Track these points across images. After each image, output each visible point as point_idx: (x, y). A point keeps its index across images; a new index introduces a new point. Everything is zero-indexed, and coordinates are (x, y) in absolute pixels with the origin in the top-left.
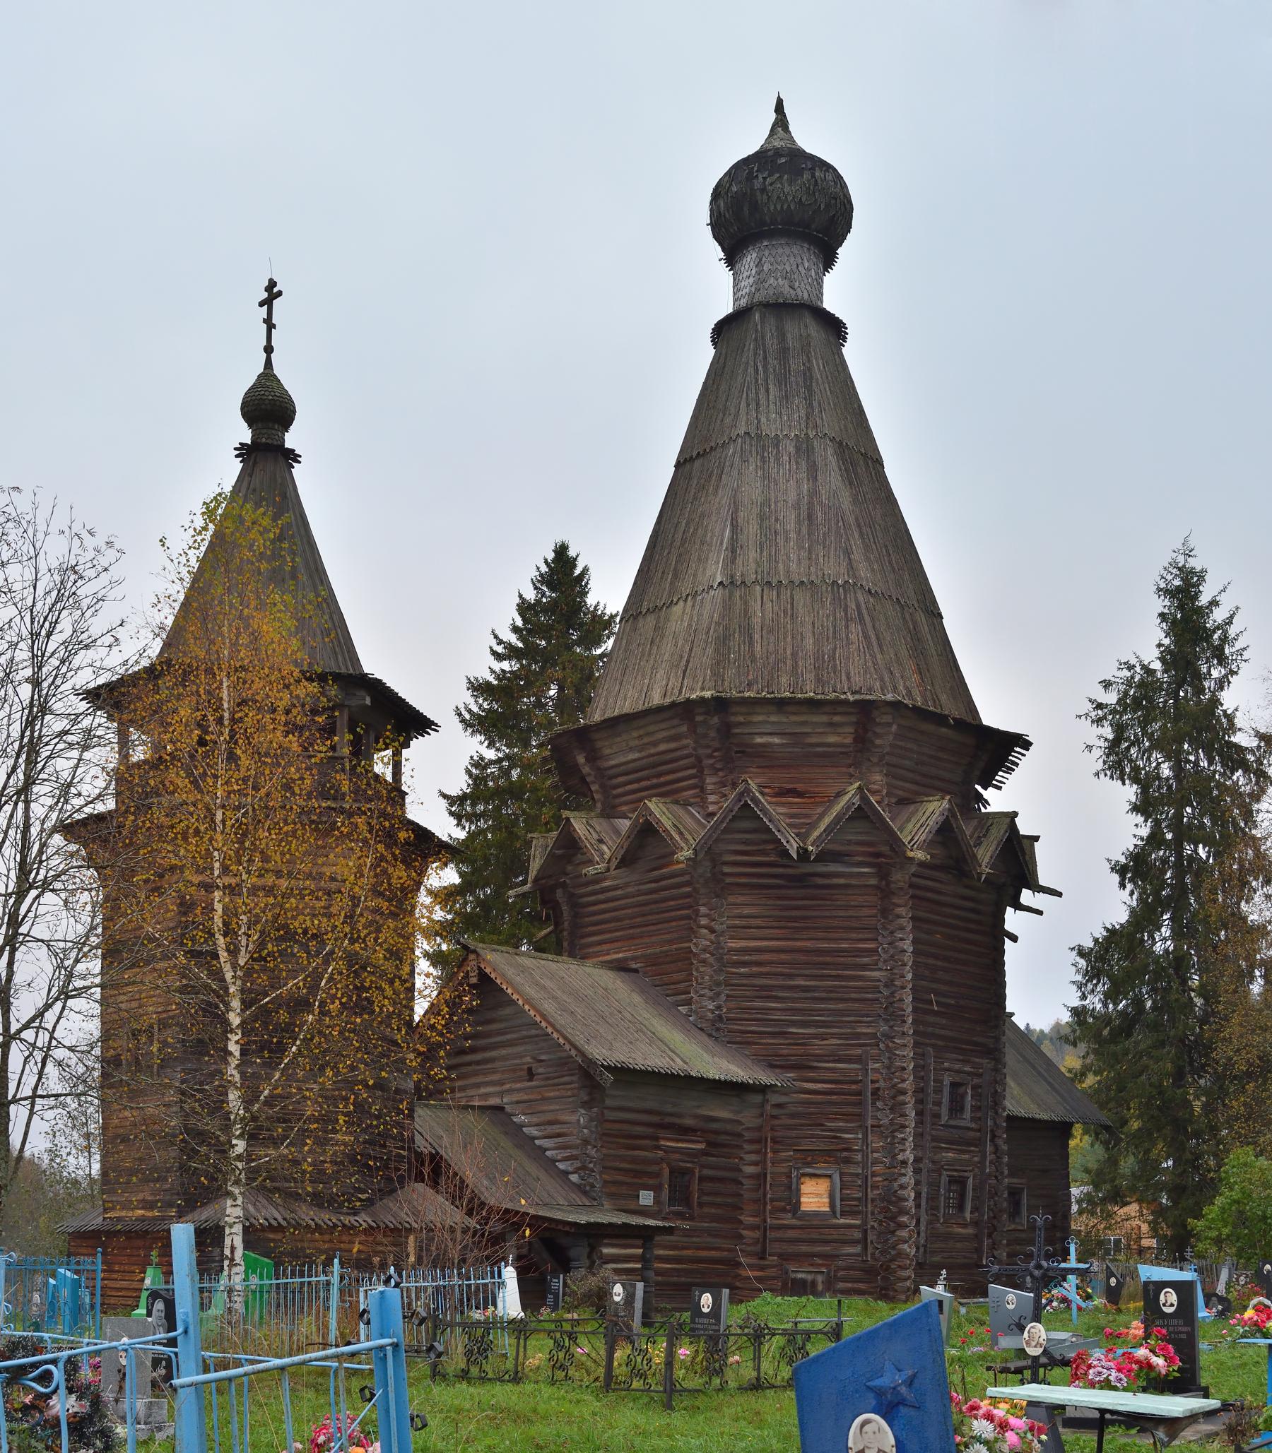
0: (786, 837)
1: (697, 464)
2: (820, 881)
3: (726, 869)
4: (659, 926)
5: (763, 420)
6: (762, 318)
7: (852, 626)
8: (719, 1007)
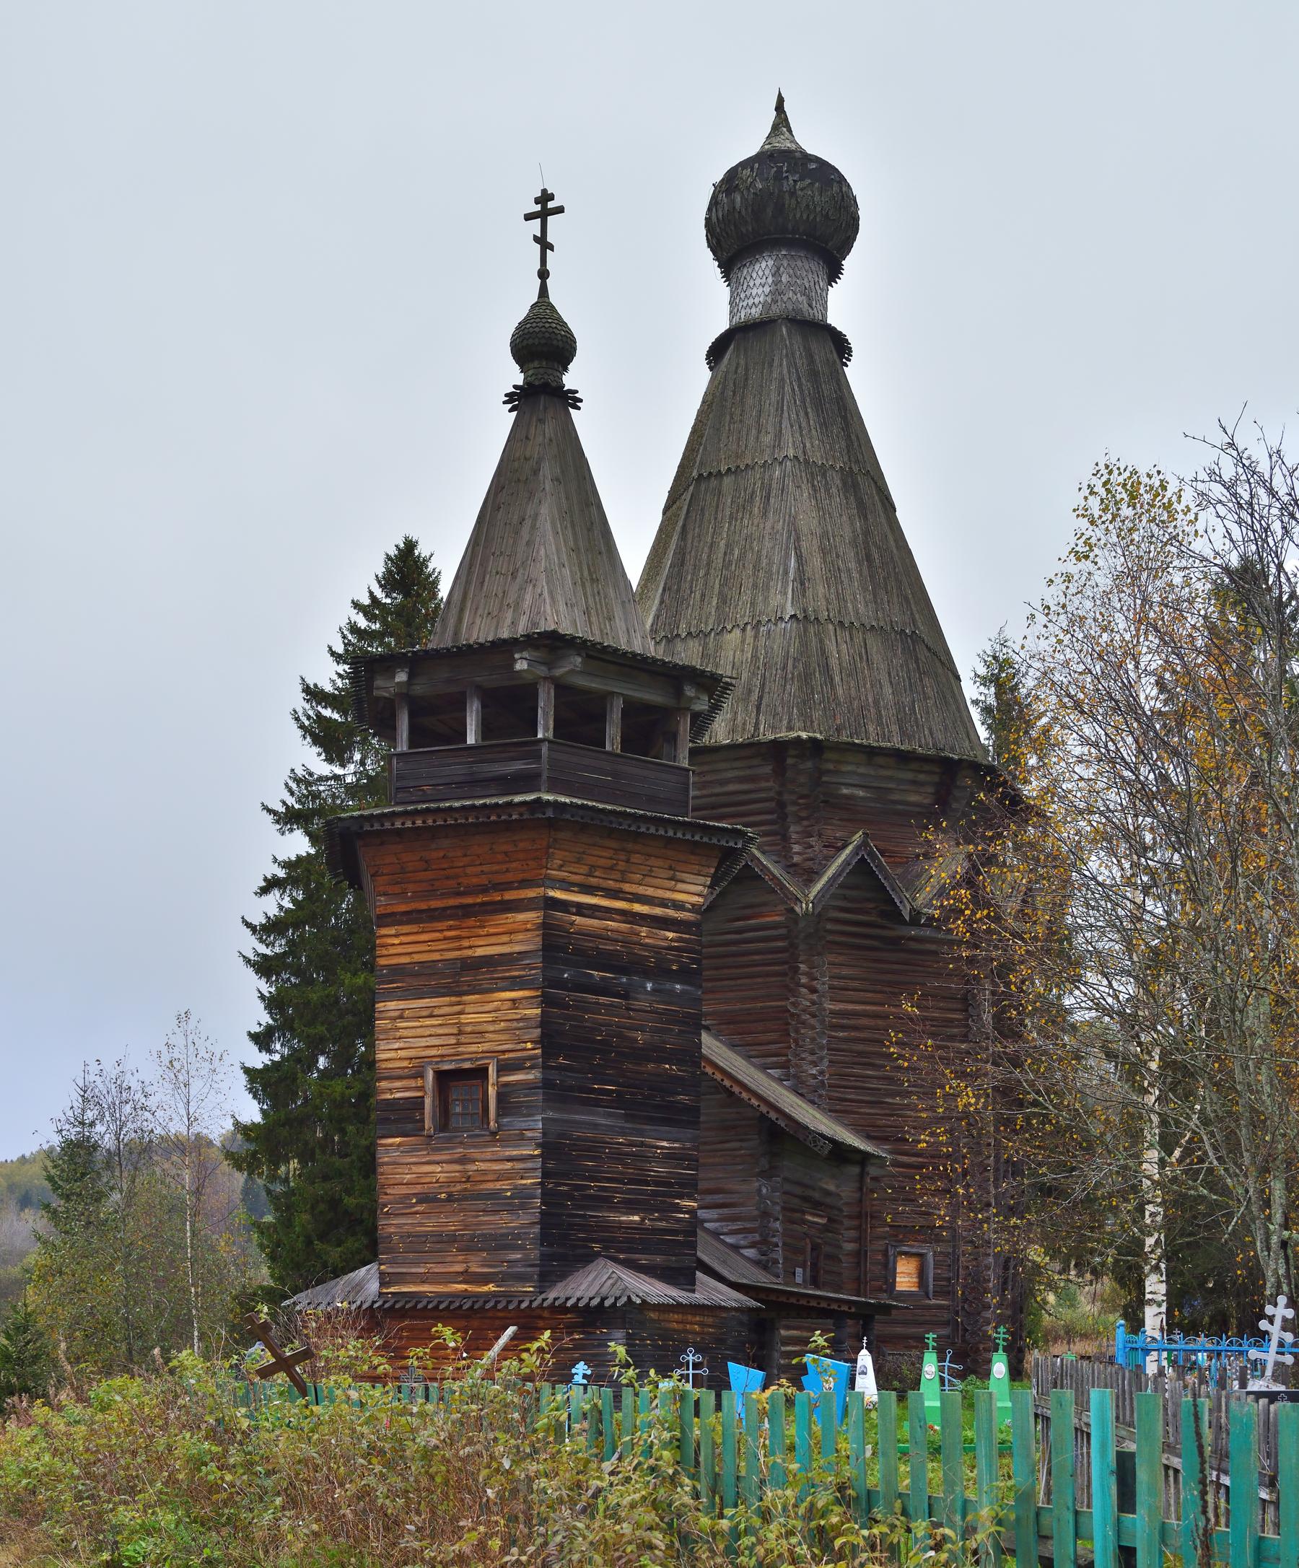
0: (900, 897)
1: (727, 481)
2: (914, 945)
3: (829, 926)
4: (739, 982)
5: (808, 445)
6: (789, 333)
7: (926, 681)
8: (822, 1073)
